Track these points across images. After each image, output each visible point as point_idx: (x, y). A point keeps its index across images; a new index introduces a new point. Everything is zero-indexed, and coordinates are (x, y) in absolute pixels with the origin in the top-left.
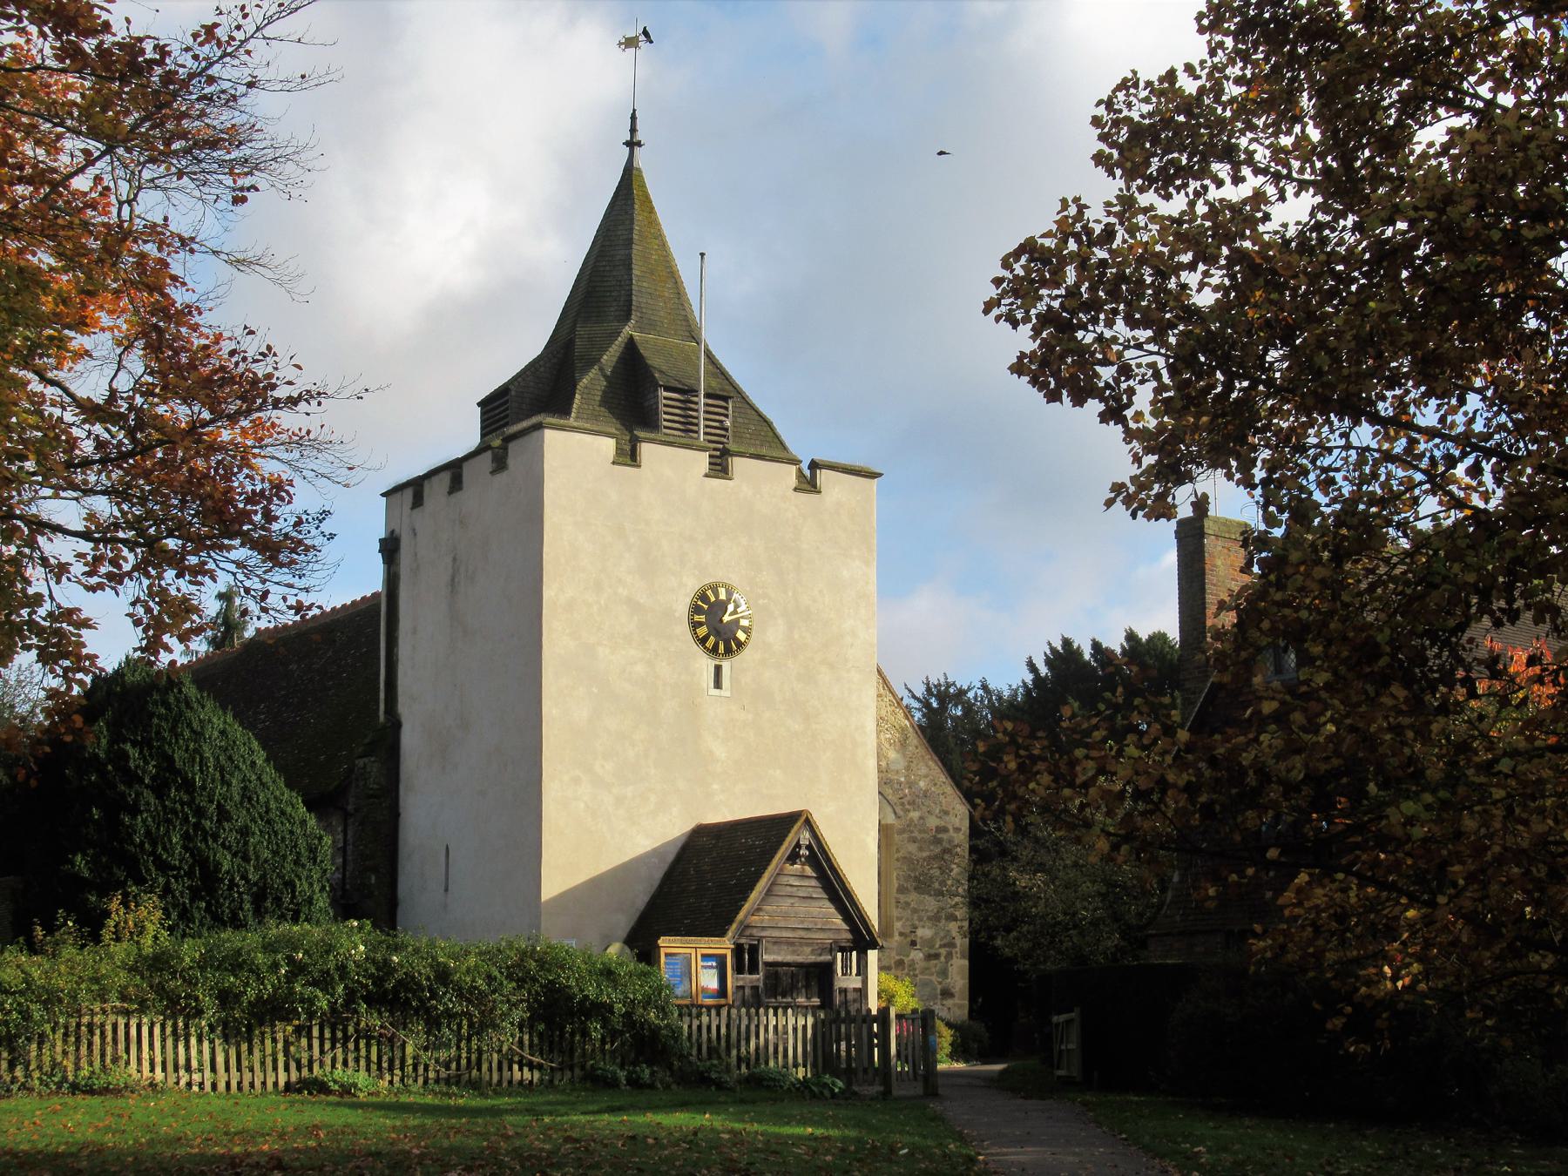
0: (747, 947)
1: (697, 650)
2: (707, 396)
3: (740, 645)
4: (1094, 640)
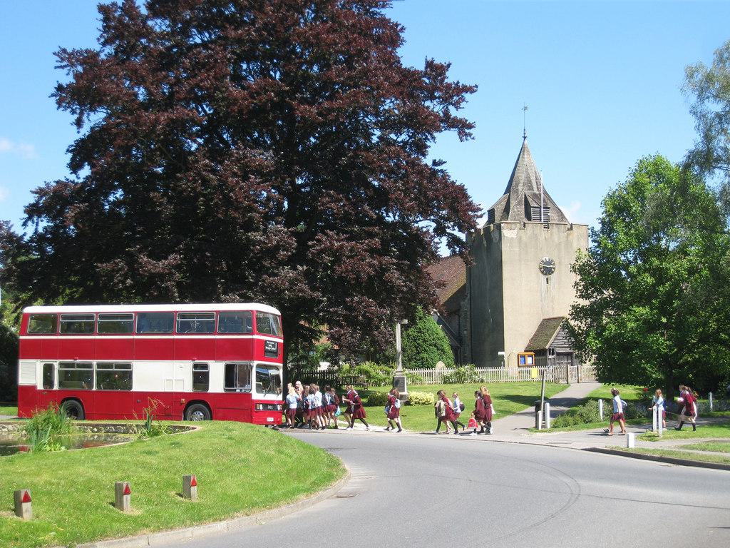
1: (540, 274)
2: (544, 208)
3: (553, 272)
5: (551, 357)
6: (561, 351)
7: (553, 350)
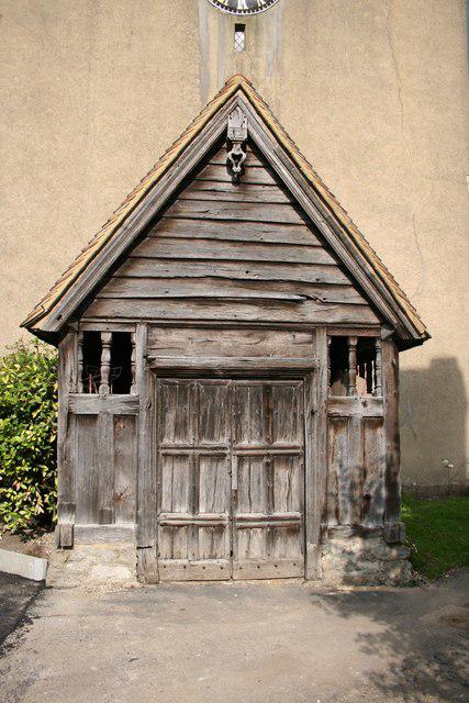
0: (107, 337)
7: (122, 344)
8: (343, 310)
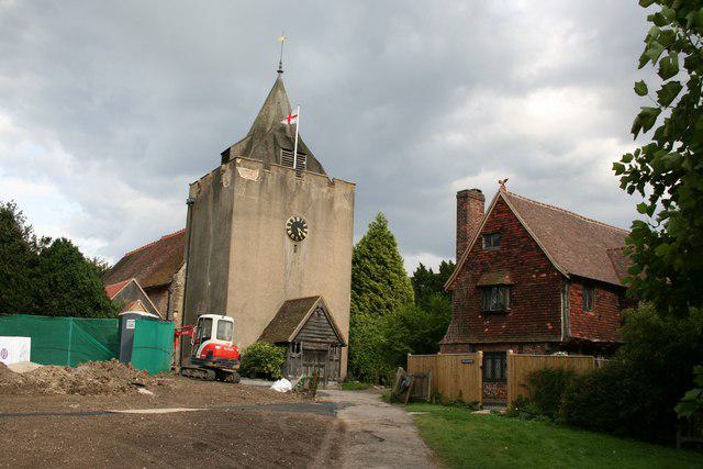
1: (287, 237)
4: (379, 219)
5: (295, 355)
6: (310, 347)
7: (299, 344)
8: (332, 339)
